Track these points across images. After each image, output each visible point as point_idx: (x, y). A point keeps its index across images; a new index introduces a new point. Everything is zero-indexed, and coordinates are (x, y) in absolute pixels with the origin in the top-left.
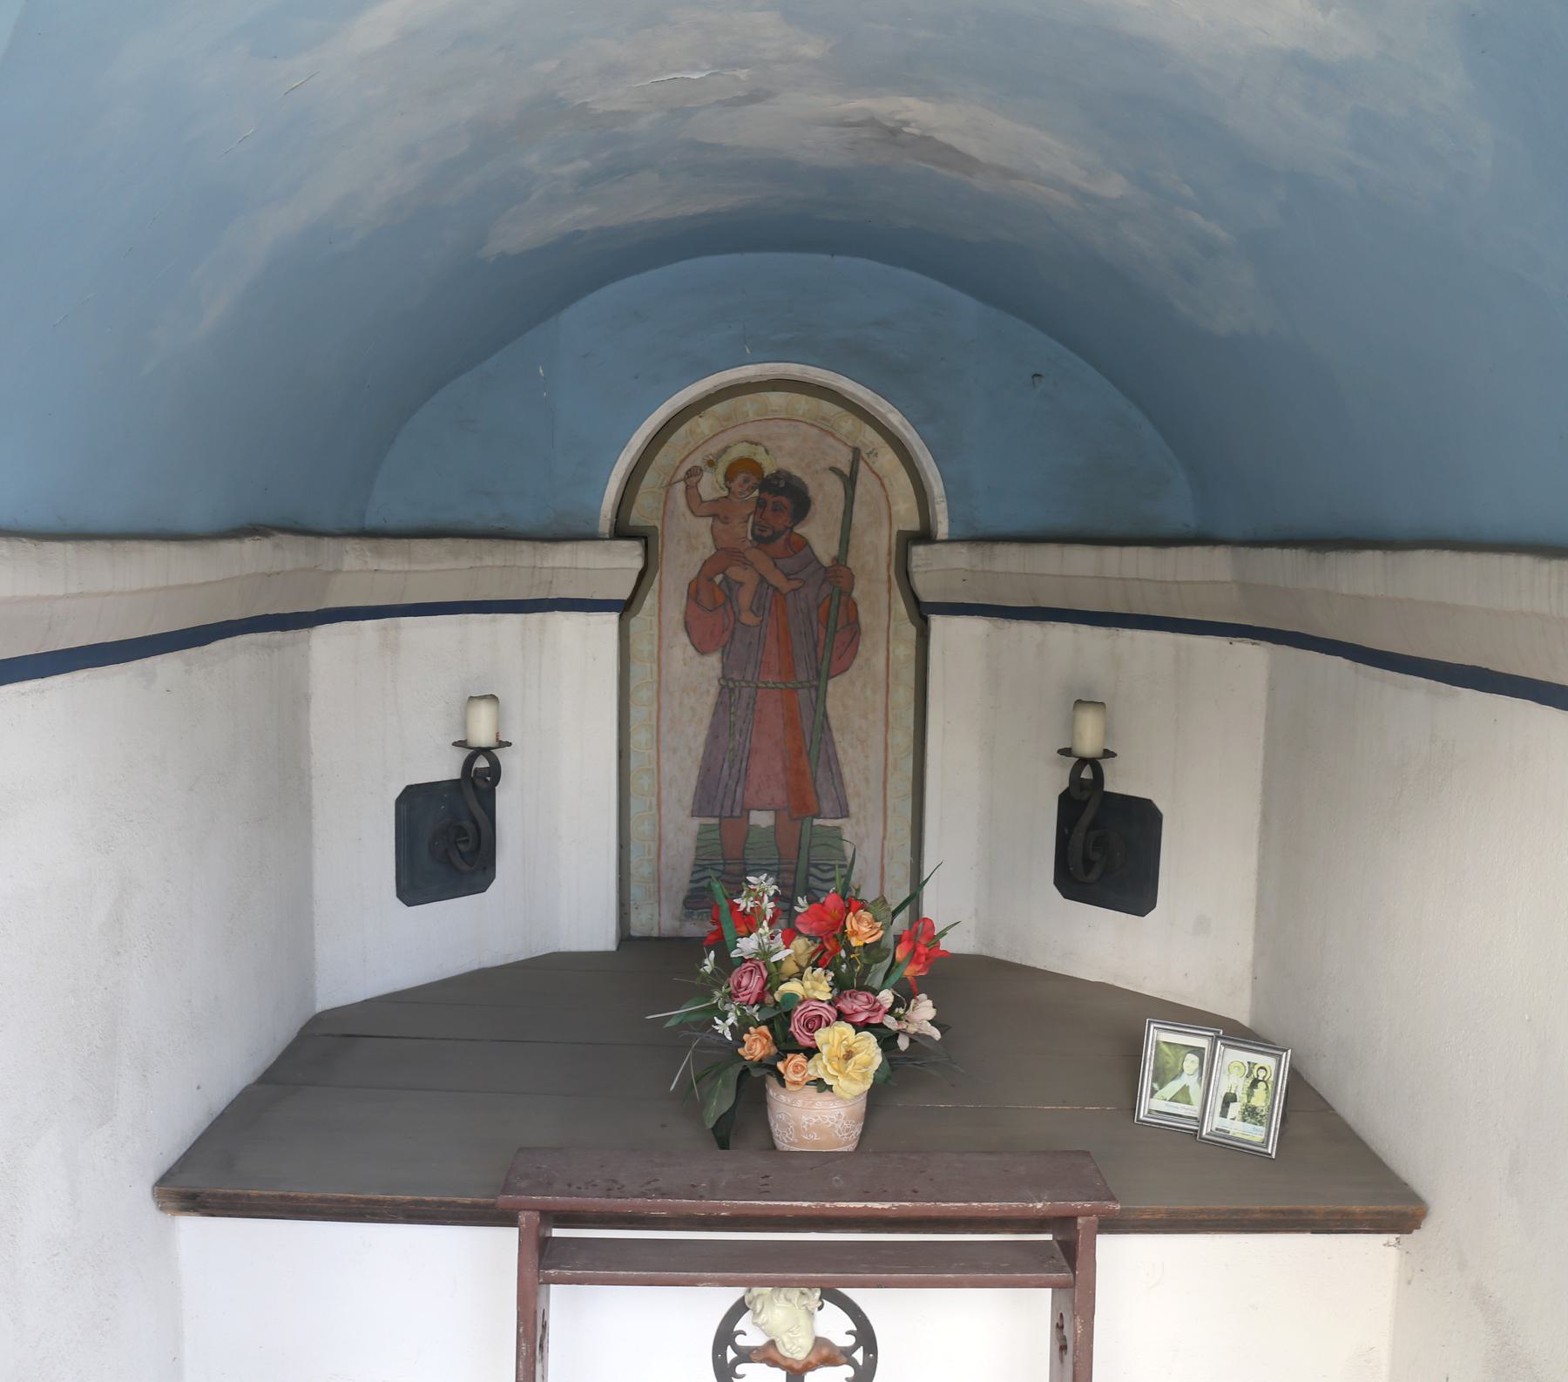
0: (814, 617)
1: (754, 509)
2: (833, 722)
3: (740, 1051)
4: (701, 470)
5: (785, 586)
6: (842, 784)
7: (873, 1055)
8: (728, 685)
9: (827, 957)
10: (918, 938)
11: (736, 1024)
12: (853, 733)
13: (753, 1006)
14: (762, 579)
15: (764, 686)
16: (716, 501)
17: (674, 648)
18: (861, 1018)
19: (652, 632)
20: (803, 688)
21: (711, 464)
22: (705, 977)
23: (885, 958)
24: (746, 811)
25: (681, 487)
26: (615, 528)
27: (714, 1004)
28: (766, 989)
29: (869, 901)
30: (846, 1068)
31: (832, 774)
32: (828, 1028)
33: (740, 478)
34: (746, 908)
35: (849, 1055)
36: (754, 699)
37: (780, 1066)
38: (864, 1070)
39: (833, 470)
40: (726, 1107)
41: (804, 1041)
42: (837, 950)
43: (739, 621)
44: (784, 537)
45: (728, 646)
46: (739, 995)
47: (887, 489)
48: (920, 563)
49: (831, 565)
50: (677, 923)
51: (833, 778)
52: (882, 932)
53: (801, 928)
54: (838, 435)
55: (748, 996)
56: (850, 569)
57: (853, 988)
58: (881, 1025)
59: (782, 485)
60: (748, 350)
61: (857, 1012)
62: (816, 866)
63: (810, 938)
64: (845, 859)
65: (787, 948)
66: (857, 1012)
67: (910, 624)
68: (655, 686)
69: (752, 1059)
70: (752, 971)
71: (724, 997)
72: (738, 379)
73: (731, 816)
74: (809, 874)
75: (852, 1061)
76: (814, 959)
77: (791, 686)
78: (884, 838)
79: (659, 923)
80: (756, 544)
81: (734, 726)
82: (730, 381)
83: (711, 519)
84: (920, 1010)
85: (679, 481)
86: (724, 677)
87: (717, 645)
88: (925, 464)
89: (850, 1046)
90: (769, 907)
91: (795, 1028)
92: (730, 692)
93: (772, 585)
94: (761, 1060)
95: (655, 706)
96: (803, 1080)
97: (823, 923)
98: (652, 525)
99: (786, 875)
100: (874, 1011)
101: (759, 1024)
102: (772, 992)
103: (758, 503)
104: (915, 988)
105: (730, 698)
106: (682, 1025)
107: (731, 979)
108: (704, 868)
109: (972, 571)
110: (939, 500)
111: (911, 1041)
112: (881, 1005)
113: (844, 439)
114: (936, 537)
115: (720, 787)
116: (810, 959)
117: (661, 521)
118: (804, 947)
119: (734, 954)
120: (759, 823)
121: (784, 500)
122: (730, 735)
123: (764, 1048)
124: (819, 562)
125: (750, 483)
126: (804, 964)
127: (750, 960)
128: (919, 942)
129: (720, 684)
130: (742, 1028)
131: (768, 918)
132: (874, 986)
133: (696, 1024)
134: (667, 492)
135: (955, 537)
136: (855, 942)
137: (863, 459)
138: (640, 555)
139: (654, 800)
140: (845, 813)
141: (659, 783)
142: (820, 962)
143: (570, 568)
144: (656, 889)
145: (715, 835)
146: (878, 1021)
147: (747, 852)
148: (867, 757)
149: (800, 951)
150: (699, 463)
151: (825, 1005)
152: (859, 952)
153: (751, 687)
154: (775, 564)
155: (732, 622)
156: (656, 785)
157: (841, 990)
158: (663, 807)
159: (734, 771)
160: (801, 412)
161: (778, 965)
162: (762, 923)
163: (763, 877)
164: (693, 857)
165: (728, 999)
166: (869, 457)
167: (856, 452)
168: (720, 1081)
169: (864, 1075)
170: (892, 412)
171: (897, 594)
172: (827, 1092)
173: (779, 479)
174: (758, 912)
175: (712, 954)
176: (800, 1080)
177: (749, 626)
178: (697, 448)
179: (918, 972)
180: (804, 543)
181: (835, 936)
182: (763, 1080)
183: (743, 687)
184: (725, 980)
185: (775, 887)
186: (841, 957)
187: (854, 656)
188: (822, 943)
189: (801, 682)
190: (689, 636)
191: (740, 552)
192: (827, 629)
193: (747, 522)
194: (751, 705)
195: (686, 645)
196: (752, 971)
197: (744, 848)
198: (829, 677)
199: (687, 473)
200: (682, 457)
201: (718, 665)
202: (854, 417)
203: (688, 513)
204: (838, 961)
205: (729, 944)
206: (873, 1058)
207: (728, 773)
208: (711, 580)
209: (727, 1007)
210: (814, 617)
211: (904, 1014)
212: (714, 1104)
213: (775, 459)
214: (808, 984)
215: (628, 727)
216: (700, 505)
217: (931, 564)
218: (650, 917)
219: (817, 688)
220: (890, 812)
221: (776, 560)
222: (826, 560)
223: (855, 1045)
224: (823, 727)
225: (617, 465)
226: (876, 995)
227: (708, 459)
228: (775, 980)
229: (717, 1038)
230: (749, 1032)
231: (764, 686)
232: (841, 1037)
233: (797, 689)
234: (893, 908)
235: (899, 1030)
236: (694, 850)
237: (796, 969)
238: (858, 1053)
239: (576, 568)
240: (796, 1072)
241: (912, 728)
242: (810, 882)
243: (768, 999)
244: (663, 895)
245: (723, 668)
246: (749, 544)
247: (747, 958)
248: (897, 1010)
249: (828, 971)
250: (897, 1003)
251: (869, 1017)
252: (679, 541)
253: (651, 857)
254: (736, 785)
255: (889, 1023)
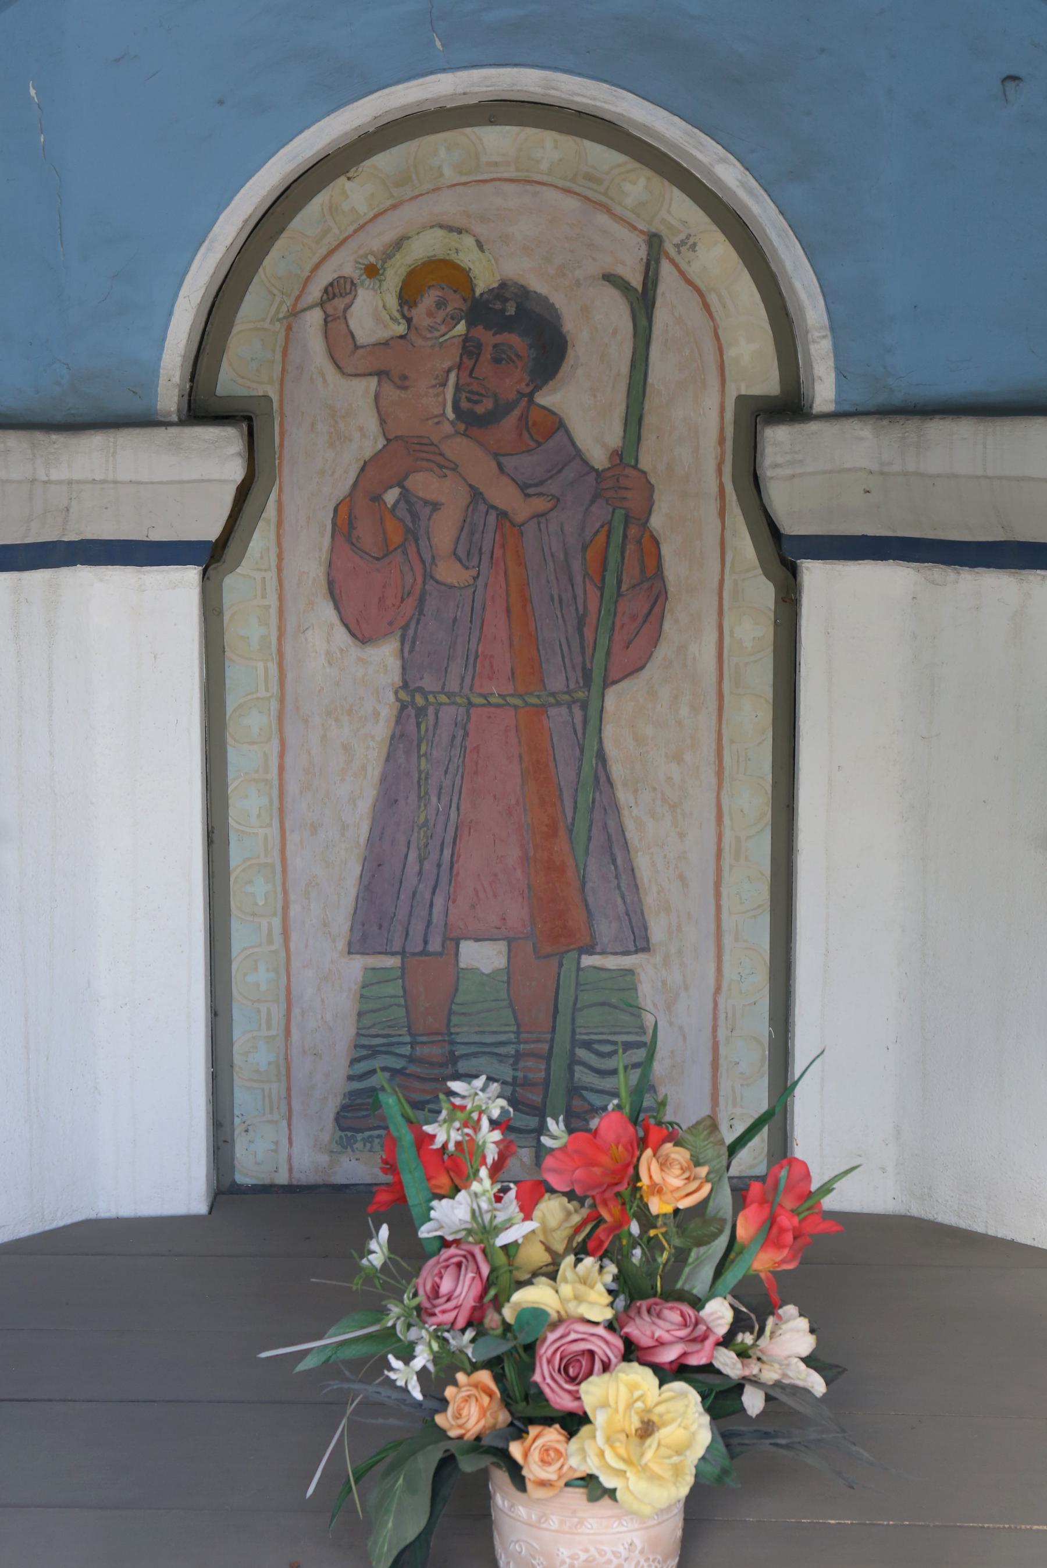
0: (576, 565)
1: (458, 359)
2: (617, 770)
3: (439, 1419)
4: (353, 284)
5: (521, 508)
6: (636, 887)
7: (694, 1427)
8: (413, 702)
9: (603, 1237)
10: (778, 1200)
11: (431, 1367)
12: (655, 789)
13: (463, 1331)
14: (476, 495)
15: (482, 701)
16: (385, 344)
17: (309, 633)
18: (669, 1355)
19: (266, 602)
20: (558, 704)
21: (372, 271)
22: (370, 1277)
23: (715, 1236)
24: (453, 942)
25: (314, 318)
26: (189, 401)
27: (389, 1328)
28: (487, 1299)
29: (684, 1127)
30: (642, 1455)
31: (616, 867)
32: (606, 1376)
33: (429, 300)
34: (445, 1146)
35: (647, 1429)
36: (464, 728)
37: (515, 1449)
38: (676, 1459)
39: (610, 279)
40: (411, 1532)
41: (562, 1401)
42: (621, 1223)
43: (432, 577)
44: (516, 413)
45: (413, 625)
46: (437, 1310)
47: (715, 315)
48: (780, 460)
49: (607, 465)
50: (324, 1159)
51: (617, 877)
52: (707, 1188)
53: (553, 1180)
54: (618, 210)
55: (454, 1313)
56: (645, 473)
57: (655, 1295)
58: (709, 1368)
59: (511, 310)
60: (438, 44)
61: (661, 1343)
62: (587, 1045)
63: (570, 1195)
64: (642, 1030)
65: (528, 1217)
66: (661, 1343)
67: (763, 578)
68: (274, 705)
69: (460, 1437)
70: (459, 1265)
71: (408, 1316)
72: (420, 103)
73: (424, 953)
74: (573, 1061)
75: (652, 1442)
76: (580, 1238)
77: (534, 700)
78: (718, 990)
79: (290, 1158)
80: (462, 427)
81: (426, 779)
82: (404, 107)
83: (373, 381)
84: (788, 1336)
85: (310, 308)
86: (405, 685)
87: (390, 624)
88: (789, 265)
89: (649, 1411)
90: (490, 1139)
91: (543, 1375)
92: (417, 716)
93: (494, 507)
94: (478, 1438)
95: (275, 743)
96: (560, 1477)
97: (597, 1170)
98: (261, 394)
99: (530, 1063)
100: (694, 1340)
101: (475, 1367)
102: (498, 1304)
103: (464, 348)
104: (775, 1296)
105: (418, 725)
106: (329, 1369)
107: (420, 1280)
108: (374, 1052)
109: (882, 473)
110: (816, 334)
111: (768, 1398)
112: (708, 1328)
113: (630, 216)
114: (811, 407)
115: (402, 896)
116: (571, 1239)
117: (277, 386)
118: (559, 1215)
119: (425, 1232)
120: (476, 964)
121: (515, 341)
122: (420, 798)
123: (484, 1416)
124: (585, 462)
125: (449, 309)
126: (560, 1248)
127: (457, 1242)
128: (780, 1206)
129: (398, 700)
130: (442, 1375)
131: (489, 1161)
132: (695, 1292)
133: (354, 1365)
134: (289, 328)
135: (847, 407)
136: (657, 1206)
137: (668, 256)
138: (239, 454)
139: (277, 922)
140: (642, 944)
141: (285, 891)
142: (591, 1245)
143: (103, 482)
144: (284, 1094)
145: (394, 989)
146: (703, 1361)
147: (455, 1020)
148: (681, 835)
149: (552, 1223)
150: (349, 270)
151: (601, 1331)
152: (665, 1224)
153: (460, 705)
154: (501, 467)
155: (419, 580)
156: (280, 896)
157: (632, 1299)
158: (294, 936)
159: (427, 866)
160: (544, 166)
161: (512, 1251)
162: (478, 1171)
163: (479, 1082)
164: (352, 1031)
165: (414, 1319)
166: (679, 252)
167: (654, 242)
168: (401, 1481)
169: (677, 1471)
170: (723, 160)
171: (736, 517)
172: (606, 1501)
173: (506, 300)
174: (469, 1149)
175: (384, 1231)
176: (553, 1477)
177: (451, 587)
178: (345, 240)
179: (780, 1263)
180: (557, 425)
181: (618, 1194)
182: (482, 1479)
183: (441, 704)
184: (409, 1282)
185: (502, 1102)
186: (630, 1234)
187: (656, 639)
188: (594, 1206)
189: (553, 694)
190: (337, 608)
191: (432, 444)
192: (602, 589)
193: (444, 384)
194: (459, 740)
195: (332, 626)
196: (459, 1265)
197: (450, 1013)
198: (608, 682)
199: (326, 291)
200: (316, 259)
201: (394, 664)
202: (649, 173)
203: (330, 370)
204: (624, 1242)
205: (415, 1212)
206: (694, 1434)
207: (417, 868)
208: (377, 499)
209: (413, 1334)
210: (576, 565)
211: (754, 1345)
212: (390, 1525)
213: (497, 260)
214: (566, 1289)
215: (225, 785)
216: (353, 353)
217: (801, 461)
218: (273, 1147)
219: (584, 706)
220: (727, 941)
221: (503, 460)
222: (598, 458)
223: (661, 1409)
224: (597, 779)
225: (189, 278)
226: (698, 1311)
227: (366, 262)
228: (504, 1280)
229: (395, 1395)
230: (455, 1383)
231: (482, 701)
232: (632, 1392)
233: (543, 708)
234: (730, 1138)
235: (744, 1378)
236: (354, 1017)
237: (545, 1258)
238: (665, 1424)
239: (115, 482)
240: (545, 1462)
241: (769, 778)
242: (577, 1075)
243: (491, 1319)
244: (296, 1106)
245: (404, 668)
246: (448, 428)
247: (450, 1238)
248: (740, 1337)
249: (606, 1261)
250: (739, 1323)
251: (685, 1354)
252: (313, 425)
253: (273, 1033)
254: (433, 893)
255: (726, 1365)
